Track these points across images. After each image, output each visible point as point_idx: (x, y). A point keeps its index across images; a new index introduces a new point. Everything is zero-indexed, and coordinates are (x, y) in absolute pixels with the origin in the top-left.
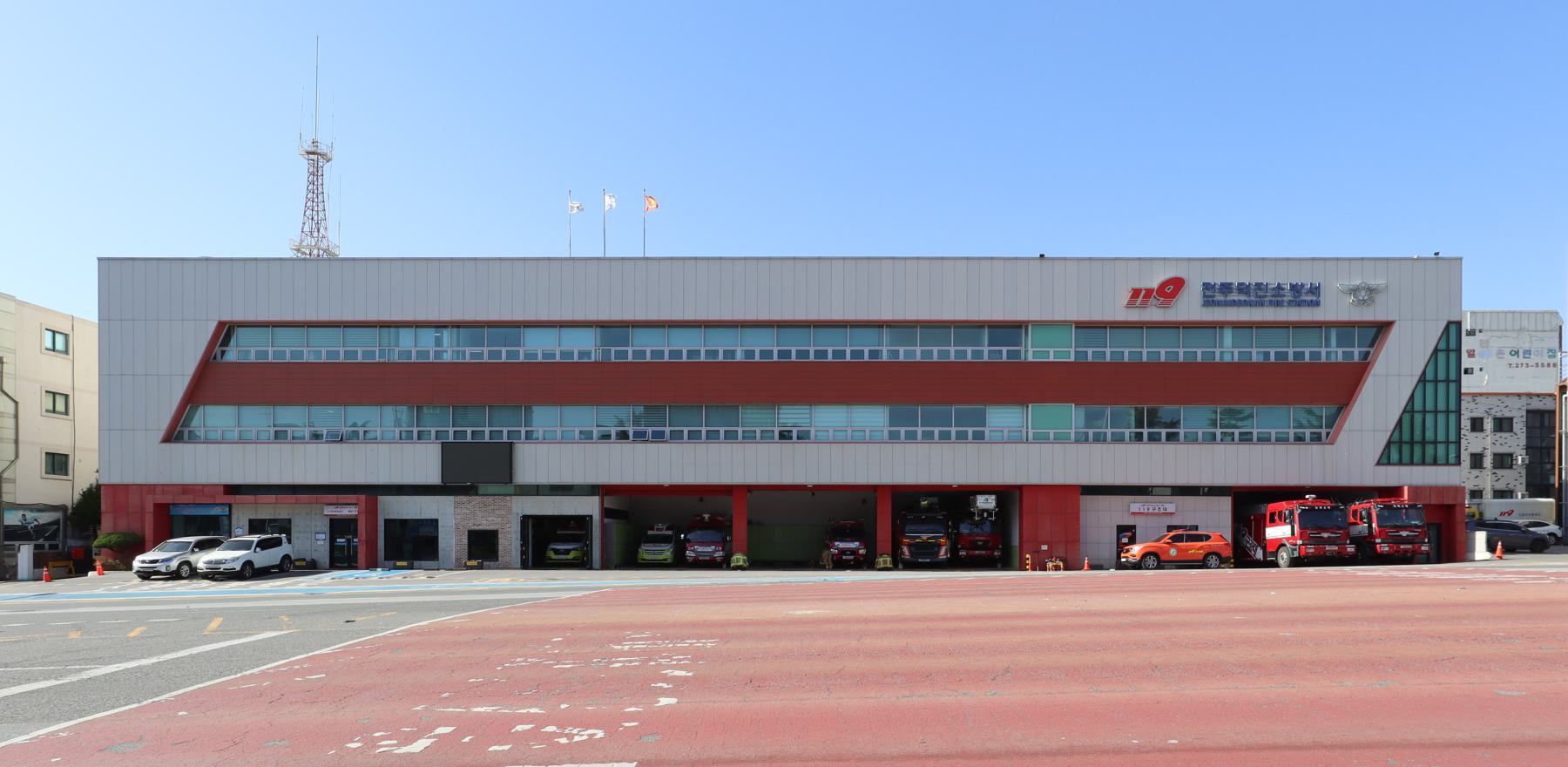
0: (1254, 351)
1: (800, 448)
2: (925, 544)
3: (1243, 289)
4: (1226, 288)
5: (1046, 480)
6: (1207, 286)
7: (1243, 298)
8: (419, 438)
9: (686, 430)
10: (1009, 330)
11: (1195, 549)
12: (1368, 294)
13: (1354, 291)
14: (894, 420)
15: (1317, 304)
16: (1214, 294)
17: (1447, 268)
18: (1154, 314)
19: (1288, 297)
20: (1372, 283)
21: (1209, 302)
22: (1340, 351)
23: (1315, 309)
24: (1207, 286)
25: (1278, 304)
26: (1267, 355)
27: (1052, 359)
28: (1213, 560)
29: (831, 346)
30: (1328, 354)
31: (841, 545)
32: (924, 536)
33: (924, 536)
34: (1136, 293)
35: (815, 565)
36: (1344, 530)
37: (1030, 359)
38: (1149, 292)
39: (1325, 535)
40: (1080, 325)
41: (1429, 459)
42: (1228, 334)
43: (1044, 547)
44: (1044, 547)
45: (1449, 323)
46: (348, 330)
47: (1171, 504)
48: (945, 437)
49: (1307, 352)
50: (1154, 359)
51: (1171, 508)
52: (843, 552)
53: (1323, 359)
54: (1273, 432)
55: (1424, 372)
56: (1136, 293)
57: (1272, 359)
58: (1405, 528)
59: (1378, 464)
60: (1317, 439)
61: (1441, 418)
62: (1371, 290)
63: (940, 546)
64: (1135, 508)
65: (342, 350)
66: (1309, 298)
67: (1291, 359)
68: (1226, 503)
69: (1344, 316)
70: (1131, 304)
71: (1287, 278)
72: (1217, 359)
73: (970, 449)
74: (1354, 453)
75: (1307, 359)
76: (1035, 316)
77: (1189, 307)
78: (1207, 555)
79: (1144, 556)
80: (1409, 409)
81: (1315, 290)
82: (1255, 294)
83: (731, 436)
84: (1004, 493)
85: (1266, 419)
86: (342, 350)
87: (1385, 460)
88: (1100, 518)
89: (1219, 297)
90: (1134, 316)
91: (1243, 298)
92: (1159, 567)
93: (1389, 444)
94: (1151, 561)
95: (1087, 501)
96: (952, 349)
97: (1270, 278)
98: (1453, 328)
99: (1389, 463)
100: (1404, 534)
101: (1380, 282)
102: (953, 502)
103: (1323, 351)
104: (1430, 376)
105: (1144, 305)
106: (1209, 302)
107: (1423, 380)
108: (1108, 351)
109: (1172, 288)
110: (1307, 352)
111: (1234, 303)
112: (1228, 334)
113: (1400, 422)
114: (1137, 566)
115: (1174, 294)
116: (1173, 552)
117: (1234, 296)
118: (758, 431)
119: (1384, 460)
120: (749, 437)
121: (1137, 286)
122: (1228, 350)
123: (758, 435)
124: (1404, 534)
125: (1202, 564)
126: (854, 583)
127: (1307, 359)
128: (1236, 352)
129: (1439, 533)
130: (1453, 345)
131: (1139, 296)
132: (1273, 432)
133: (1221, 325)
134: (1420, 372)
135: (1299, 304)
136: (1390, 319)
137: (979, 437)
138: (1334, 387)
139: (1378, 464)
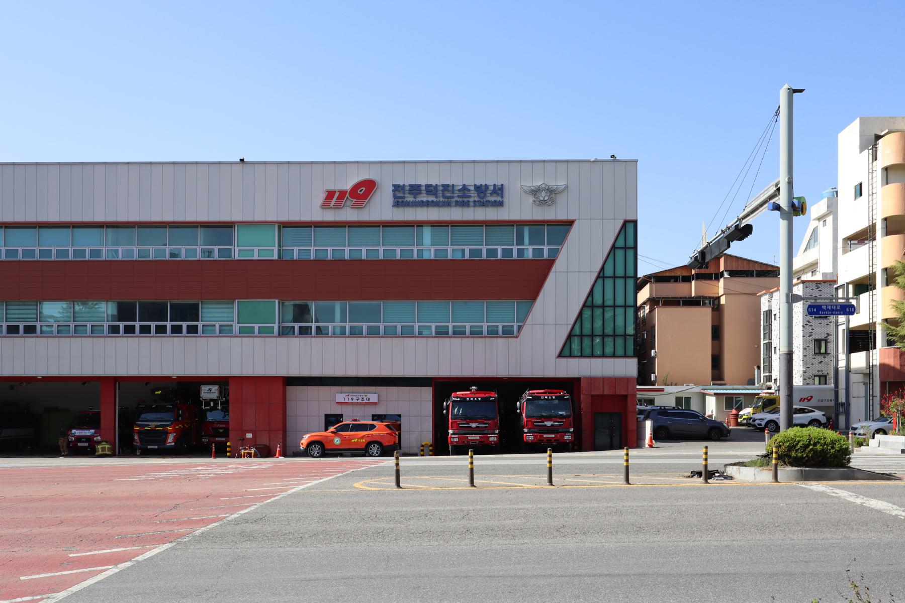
0: (450, 249)
1: (30, 342)
2: (153, 432)
3: (431, 189)
4: (415, 189)
5: (248, 372)
6: (397, 188)
7: (431, 198)
8: (76, 331)
9: (256, 326)
10: (222, 229)
11: (358, 438)
12: (549, 195)
13: (535, 192)
14: (113, 316)
15: (500, 204)
16: (404, 195)
17: (622, 170)
18: (349, 214)
19: (474, 197)
20: (552, 183)
21: (399, 203)
22: (530, 248)
23: (500, 209)
24: (397, 188)
25: (464, 204)
26: (210, 252)
27: (256, 257)
28: (375, 449)
29: (57, 246)
30: (521, 252)
31: (77, 432)
32: (153, 424)
33: (153, 424)
34: (330, 195)
35: (54, 452)
36: (494, 417)
37: (237, 258)
38: (342, 194)
39: (474, 425)
40: (284, 225)
41: (587, 351)
42: (427, 232)
43: (249, 436)
44: (249, 436)
45: (626, 222)
46: (76, 230)
47: (372, 394)
48: (161, 330)
49: (499, 249)
50: (372, 257)
51: (373, 398)
52: (79, 439)
53: (515, 256)
54: (468, 325)
55: (603, 269)
56: (330, 195)
57: (467, 256)
58: (548, 418)
59: (560, 356)
60: (508, 333)
61: (620, 311)
62: (551, 191)
63: (167, 433)
64: (340, 398)
65: (71, 249)
66: (492, 199)
67: (515, 256)
68: (427, 393)
69: (527, 216)
70: (325, 206)
71: (471, 179)
72: (415, 257)
73: (177, 342)
74: (535, 345)
75: (500, 256)
76: (240, 219)
77: (380, 208)
78: (369, 444)
79: (310, 444)
80: (589, 304)
81: (499, 190)
82: (443, 195)
83: (373, 333)
84: (223, 382)
85: (395, 312)
86: (71, 249)
87: (566, 352)
88: (308, 411)
89: (410, 198)
90: (330, 216)
91: (431, 198)
92: (324, 455)
93: (570, 336)
94: (316, 450)
95: (292, 391)
96: (546, 248)
97: (457, 180)
98: (630, 227)
99: (571, 356)
100: (549, 424)
101: (560, 183)
102: (182, 392)
103: (515, 248)
104: (609, 272)
105: (337, 207)
106: (399, 203)
107: (601, 275)
108: (313, 249)
109: (365, 190)
110: (499, 249)
111: (427, 204)
112: (427, 232)
113: (580, 315)
114: (306, 453)
115: (365, 196)
116: (337, 441)
117: (424, 198)
118: (89, 325)
119: (565, 352)
120: (390, 333)
121: (332, 188)
122: (427, 247)
123: (256, 330)
124: (549, 424)
125: (363, 452)
126: (112, 467)
127: (500, 256)
128: (433, 249)
129: (597, 419)
130: (630, 243)
131: (332, 197)
132: (468, 325)
133: (420, 224)
134: (598, 268)
135: (483, 204)
136: (570, 218)
137: (193, 330)
138: (522, 281)
139: (560, 356)
